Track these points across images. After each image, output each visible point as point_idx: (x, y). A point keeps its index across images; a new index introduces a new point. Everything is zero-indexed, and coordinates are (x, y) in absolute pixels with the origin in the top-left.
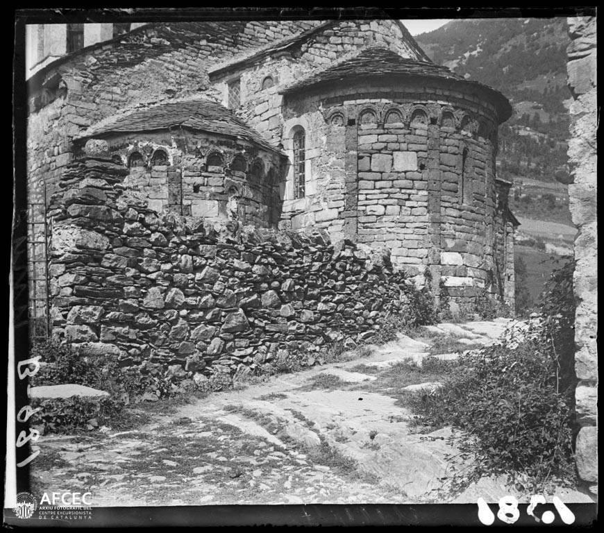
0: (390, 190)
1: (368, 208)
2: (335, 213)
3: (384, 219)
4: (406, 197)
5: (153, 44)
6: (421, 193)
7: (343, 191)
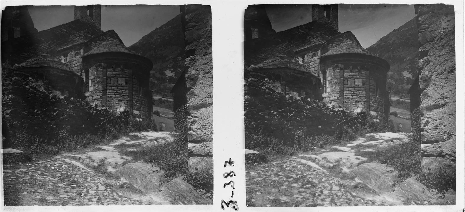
0: (354, 91)
1: (347, 96)
3: (115, 99)
4: (122, 92)
6: (363, 92)
7: (339, 91)
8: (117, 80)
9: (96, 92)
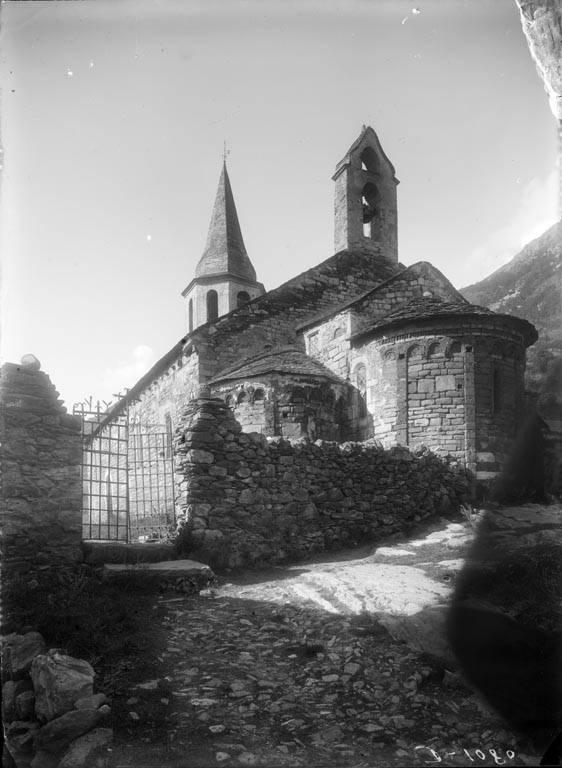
0: (433, 406)
1: (416, 421)
2: (389, 427)
5: (257, 314)
8: (435, 383)
9: (382, 417)
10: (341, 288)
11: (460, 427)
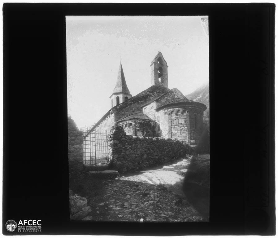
10: (153, 95)
11: (186, 133)
